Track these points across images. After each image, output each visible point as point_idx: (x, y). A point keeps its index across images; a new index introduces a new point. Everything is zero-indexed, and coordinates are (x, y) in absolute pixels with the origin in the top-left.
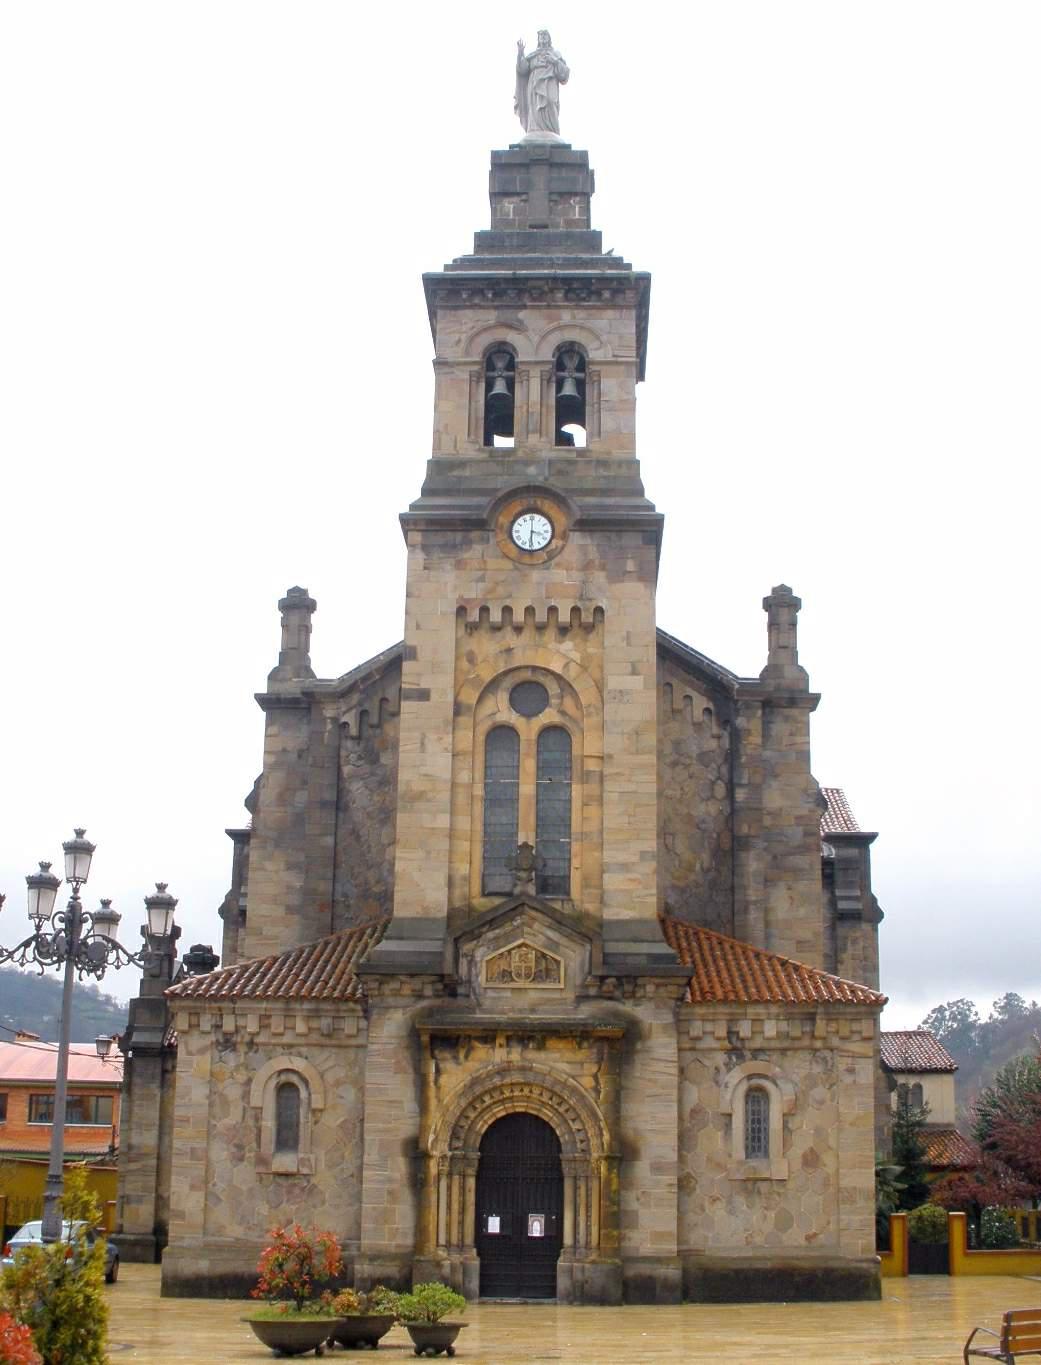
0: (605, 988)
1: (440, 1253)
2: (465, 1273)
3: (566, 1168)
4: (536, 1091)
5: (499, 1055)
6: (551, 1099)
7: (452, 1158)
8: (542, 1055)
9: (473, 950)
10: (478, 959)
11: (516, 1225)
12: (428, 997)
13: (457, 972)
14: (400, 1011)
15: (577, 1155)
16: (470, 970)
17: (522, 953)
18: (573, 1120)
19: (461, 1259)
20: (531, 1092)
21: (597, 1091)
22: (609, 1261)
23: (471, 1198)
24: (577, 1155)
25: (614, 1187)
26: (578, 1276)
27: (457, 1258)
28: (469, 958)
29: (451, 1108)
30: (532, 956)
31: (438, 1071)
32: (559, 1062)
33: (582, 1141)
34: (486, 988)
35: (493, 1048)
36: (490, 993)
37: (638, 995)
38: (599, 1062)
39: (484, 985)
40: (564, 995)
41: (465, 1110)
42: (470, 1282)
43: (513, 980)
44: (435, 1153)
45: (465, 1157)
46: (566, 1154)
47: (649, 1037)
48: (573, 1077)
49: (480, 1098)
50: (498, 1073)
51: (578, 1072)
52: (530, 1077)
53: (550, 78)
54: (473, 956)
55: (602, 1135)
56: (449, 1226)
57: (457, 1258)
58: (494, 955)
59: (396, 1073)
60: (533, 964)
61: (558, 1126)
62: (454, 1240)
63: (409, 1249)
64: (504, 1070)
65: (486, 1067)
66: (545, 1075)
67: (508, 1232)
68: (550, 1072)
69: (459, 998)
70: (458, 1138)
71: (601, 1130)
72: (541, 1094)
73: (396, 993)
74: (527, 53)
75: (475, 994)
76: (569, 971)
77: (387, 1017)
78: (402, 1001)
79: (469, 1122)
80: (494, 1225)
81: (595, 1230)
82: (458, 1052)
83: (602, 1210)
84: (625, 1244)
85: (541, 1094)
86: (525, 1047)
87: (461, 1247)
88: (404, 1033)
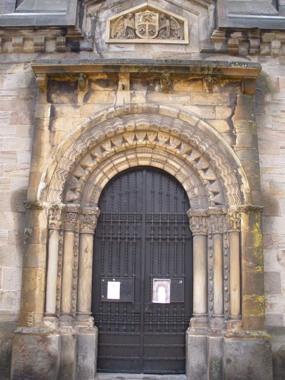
0: (230, 42)
1: (47, 323)
2: (78, 347)
3: (195, 225)
4: (163, 139)
5: (122, 98)
6: (179, 147)
7: (65, 212)
8: (170, 98)
9: (98, 12)
10: (102, 20)
11: (138, 290)
12: (51, 53)
13: (81, 27)
14: (22, 66)
15: (210, 208)
16: (94, 28)
17: (146, 14)
18: (205, 170)
19: (74, 331)
20: (156, 139)
21: (233, 137)
22: (255, 334)
23: (88, 259)
24: (210, 208)
25: (257, 244)
26: (215, 351)
27: (68, 330)
28: (93, 18)
29: (66, 154)
30: (156, 17)
31: (53, 115)
32: (187, 105)
33: (215, 194)
34: (109, 44)
35: (116, 91)
36: (113, 48)
37: (263, 52)
38: (233, 106)
39: (107, 40)
40: (188, 50)
41: (82, 156)
42: (84, 357)
43: (136, 37)
44: (45, 204)
45: (80, 213)
46: (197, 207)
47: (276, 91)
48: (205, 120)
49: (99, 144)
50: (120, 116)
51: (212, 116)
52: (157, 120)
54: (97, 17)
55: (240, 184)
56: (59, 291)
57: (68, 330)
58: (118, 15)
59: (10, 124)
60: (157, 24)
61: (187, 179)
62: (66, 309)
63: (14, 318)
64: (127, 113)
65: (107, 109)
66: (173, 119)
67: (129, 298)
68: (178, 115)
69: (82, 53)
70: (74, 190)
71: (238, 177)
72: (168, 142)
73: (19, 50)
75: (98, 49)
76: (193, 31)
77: (8, 72)
78: (24, 57)
79: (87, 173)
80: (113, 291)
81: (235, 295)
82: (77, 95)
83: (243, 273)
84: (269, 312)
85: (168, 142)
86: (151, 89)
87: (75, 316)
88: (24, 86)
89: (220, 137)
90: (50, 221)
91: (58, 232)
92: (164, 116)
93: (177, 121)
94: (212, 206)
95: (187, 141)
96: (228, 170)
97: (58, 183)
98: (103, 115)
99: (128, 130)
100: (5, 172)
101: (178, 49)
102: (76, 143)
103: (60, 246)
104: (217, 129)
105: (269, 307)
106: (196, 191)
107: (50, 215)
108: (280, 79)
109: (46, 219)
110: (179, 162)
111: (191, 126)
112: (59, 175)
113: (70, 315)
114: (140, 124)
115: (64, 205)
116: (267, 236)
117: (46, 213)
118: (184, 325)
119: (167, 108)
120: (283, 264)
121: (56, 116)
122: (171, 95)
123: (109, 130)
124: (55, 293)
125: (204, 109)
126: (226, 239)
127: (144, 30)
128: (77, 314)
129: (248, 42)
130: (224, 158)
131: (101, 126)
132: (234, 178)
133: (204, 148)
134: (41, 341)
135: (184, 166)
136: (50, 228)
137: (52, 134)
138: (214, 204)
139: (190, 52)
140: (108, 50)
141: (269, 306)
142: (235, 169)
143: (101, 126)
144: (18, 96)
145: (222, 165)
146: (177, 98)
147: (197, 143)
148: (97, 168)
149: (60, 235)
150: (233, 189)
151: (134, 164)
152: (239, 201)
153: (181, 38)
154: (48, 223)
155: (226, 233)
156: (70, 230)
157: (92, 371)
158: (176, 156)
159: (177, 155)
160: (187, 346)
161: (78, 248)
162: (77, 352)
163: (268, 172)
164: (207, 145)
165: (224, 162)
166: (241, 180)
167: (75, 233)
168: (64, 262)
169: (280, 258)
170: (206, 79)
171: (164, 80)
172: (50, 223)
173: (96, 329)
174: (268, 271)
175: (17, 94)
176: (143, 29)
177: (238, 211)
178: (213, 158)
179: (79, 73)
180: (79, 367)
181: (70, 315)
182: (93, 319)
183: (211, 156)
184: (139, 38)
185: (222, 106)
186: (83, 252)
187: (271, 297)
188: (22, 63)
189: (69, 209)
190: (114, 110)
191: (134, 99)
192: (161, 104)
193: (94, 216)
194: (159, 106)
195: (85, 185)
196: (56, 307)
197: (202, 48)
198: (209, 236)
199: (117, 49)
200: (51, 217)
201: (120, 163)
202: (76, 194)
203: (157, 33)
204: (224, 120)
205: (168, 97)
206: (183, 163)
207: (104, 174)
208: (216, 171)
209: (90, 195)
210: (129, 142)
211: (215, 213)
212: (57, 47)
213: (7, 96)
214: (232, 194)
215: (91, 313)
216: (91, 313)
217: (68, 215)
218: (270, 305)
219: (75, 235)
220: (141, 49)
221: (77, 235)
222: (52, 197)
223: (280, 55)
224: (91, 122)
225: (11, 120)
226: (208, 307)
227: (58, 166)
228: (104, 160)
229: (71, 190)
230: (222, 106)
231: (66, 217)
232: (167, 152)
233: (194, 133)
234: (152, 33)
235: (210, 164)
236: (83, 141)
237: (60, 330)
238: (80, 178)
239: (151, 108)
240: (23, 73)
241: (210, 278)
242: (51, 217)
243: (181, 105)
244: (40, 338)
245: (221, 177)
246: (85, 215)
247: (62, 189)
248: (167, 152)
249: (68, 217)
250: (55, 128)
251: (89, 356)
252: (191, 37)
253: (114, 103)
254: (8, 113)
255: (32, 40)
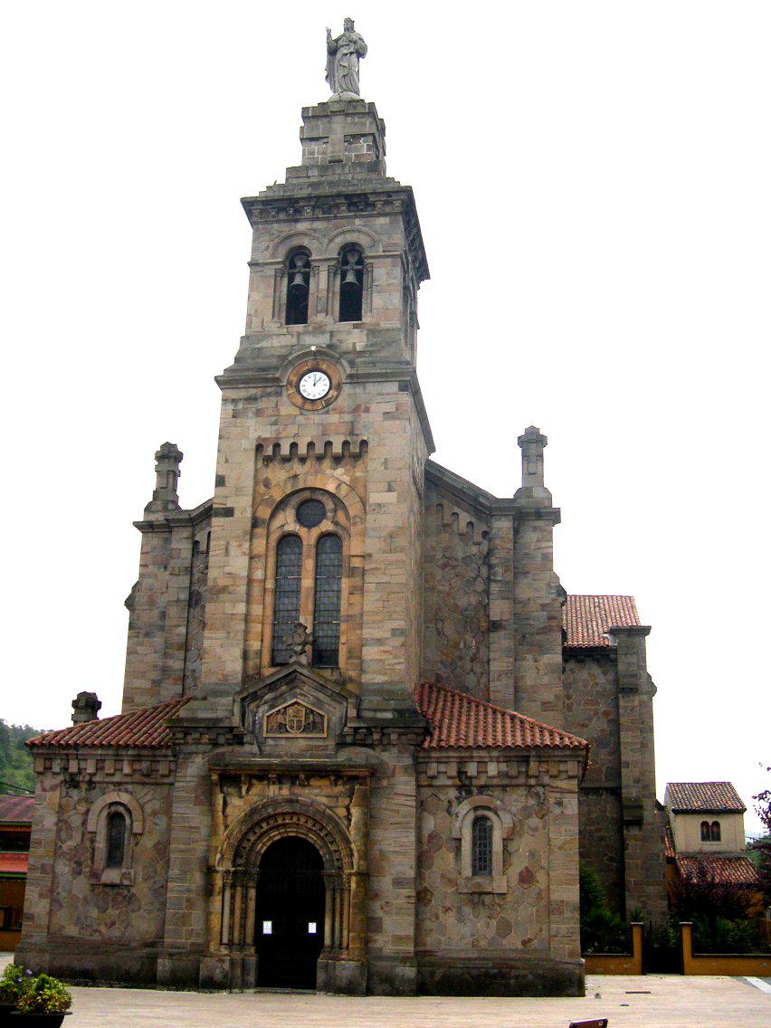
7: (235, 873)
8: (307, 791)
23: (252, 905)
29: (235, 833)
32: (318, 795)
41: (246, 833)
42: (248, 974)
45: (245, 873)
48: (330, 808)
49: (258, 824)
52: (297, 808)
53: (351, 53)
56: (231, 928)
57: (237, 955)
60: (303, 719)
62: (236, 941)
70: (241, 857)
71: (351, 850)
74: (334, 36)
78: (201, 748)
87: (242, 945)
92: (302, 805)
113: (239, 945)
161: (245, 897)
181: (239, 945)
209: (253, 859)
228: (262, 835)
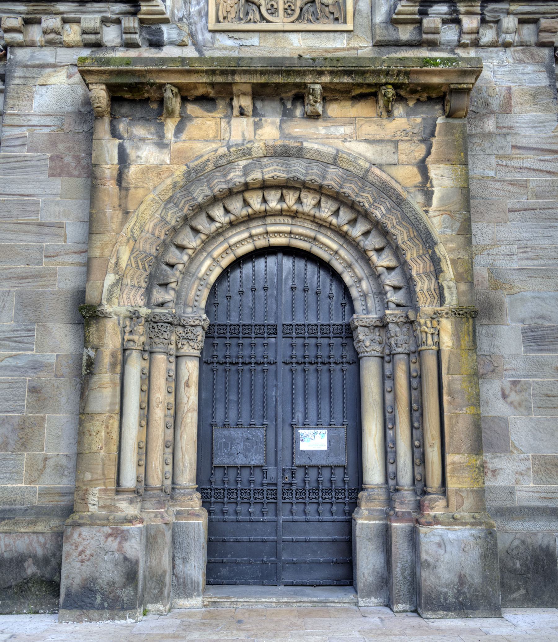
8: (320, 129)
21: (428, 195)
23: (190, 397)
32: (351, 139)
35: (228, 117)
42: (185, 561)
51: (393, 159)
52: (298, 169)
56: (144, 450)
59: (51, 175)
71: (435, 261)
77: (40, 81)
86: (287, 114)
89: (404, 195)
90: (127, 337)
91: (139, 355)
92: (311, 160)
93: (332, 169)
94: (392, 309)
95: (350, 203)
96: (418, 250)
97: (137, 275)
98: (208, 160)
99: (252, 186)
100: (46, 257)
101: (334, 40)
102: (164, 208)
103: (144, 377)
104: (400, 180)
105: (489, 474)
106: (365, 285)
107: (126, 327)
108: (513, 89)
109: (119, 333)
110: (336, 239)
111: (357, 177)
112: (139, 261)
114: (271, 175)
115: (149, 311)
116: (484, 357)
117: (119, 323)
118: (349, 503)
119: (316, 146)
120: (512, 403)
121: (129, 161)
122: (324, 124)
123: (220, 186)
124: (136, 454)
125: (379, 148)
126: (415, 363)
127: (275, 6)
128: (173, 489)
129: (458, 22)
130: (411, 230)
131: (205, 180)
132: (428, 262)
133: (378, 213)
134: (110, 535)
135: (345, 246)
136: (125, 347)
137: (124, 193)
138: (394, 306)
139: (356, 45)
140: (213, 44)
141: (489, 472)
142: (430, 248)
143: (205, 180)
144: (61, 128)
145: (408, 242)
146: (332, 130)
147: (367, 205)
148: (203, 249)
149: (144, 359)
150: (427, 281)
151: (261, 243)
152: (436, 300)
153: (341, 20)
154: (123, 339)
155: (414, 353)
156: (160, 350)
157: (198, 583)
158: (331, 229)
159: (333, 227)
160: (355, 539)
162: (173, 552)
163: (485, 252)
164: (382, 208)
165: (412, 236)
166: (439, 265)
167: (168, 354)
168: (151, 405)
169: (507, 392)
170: (383, 92)
171: (311, 97)
172: (126, 340)
173: (205, 513)
174: (486, 415)
175: (59, 123)
176: (274, 3)
177: (435, 316)
178: (393, 231)
179: (164, 84)
180: (176, 577)
182: (200, 496)
183: (389, 227)
184: (268, 21)
185: (409, 140)
186: (182, 386)
187: (492, 458)
188: (64, 66)
189: (158, 318)
190: (227, 152)
191: (259, 132)
192: (306, 141)
193: (200, 329)
194: (302, 143)
195: (183, 278)
196: (138, 477)
197: (378, 38)
198: (387, 358)
199: (229, 43)
200: (128, 329)
201: (240, 242)
202: (168, 293)
203: (298, 11)
204: (413, 165)
205: (317, 128)
206: (343, 240)
207: (214, 259)
208: (397, 252)
209: (192, 294)
210: (253, 206)
211: (395, 320)
212: (124, 36)
213: (40, 126)
214: (425, 290)
215: (197, 486)
216: (197, 486)
217: (156, 327)
218: (492, 471)
219: (168, 359)
220: (270, 39)
221: (172, 359)
222: (128, 298)
223: (515, 44)
224: (189, 172)
225: (50, 168)
226: (390, 476)
227: (137, 246)
229: (161, 285)
230: (409, 140)
231: (153, 330)
232: (316, 223)
233: (362, 189)
234: (289, 12)
235: (387, 240)
236: (176, 205)
237: (144, 515)
238: (175, 267)
239: (289, 147)
240: (66, 86)
241: (390, 426)
242: (128, 329)
243: (340, 142)
244: (110, 531)
245: (406, 262)
246: (184, 326)
247: (144, 285)
248: (316, 223)
249: (156, 330)
250: (128, 183)
251: (193, 558)
252: (357, 17)
253: (227, 139)
254: (45, 157)
255: (77, 21)
